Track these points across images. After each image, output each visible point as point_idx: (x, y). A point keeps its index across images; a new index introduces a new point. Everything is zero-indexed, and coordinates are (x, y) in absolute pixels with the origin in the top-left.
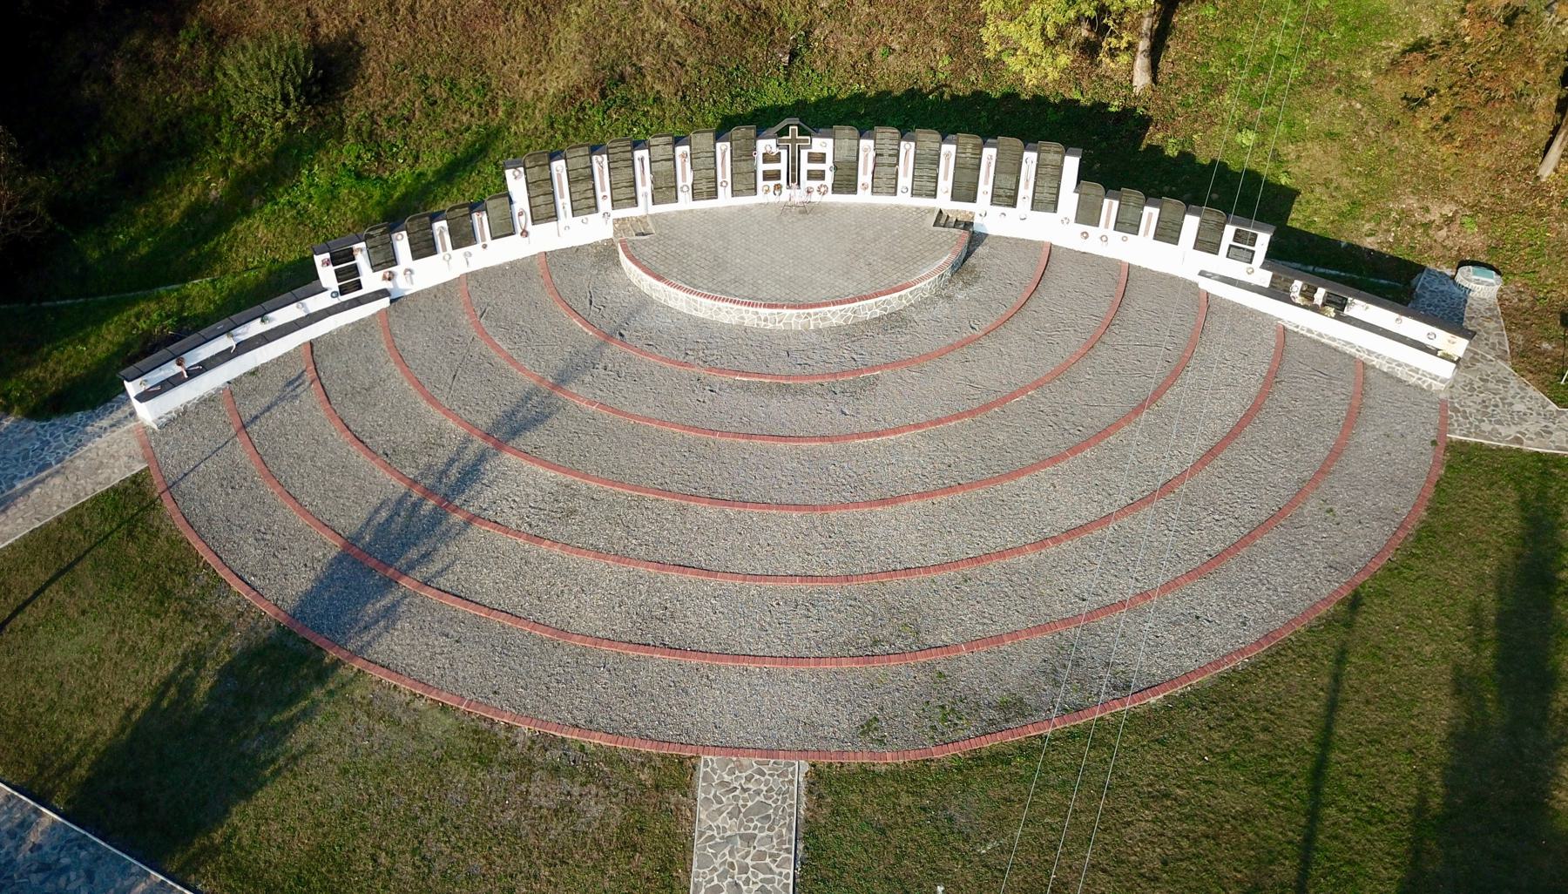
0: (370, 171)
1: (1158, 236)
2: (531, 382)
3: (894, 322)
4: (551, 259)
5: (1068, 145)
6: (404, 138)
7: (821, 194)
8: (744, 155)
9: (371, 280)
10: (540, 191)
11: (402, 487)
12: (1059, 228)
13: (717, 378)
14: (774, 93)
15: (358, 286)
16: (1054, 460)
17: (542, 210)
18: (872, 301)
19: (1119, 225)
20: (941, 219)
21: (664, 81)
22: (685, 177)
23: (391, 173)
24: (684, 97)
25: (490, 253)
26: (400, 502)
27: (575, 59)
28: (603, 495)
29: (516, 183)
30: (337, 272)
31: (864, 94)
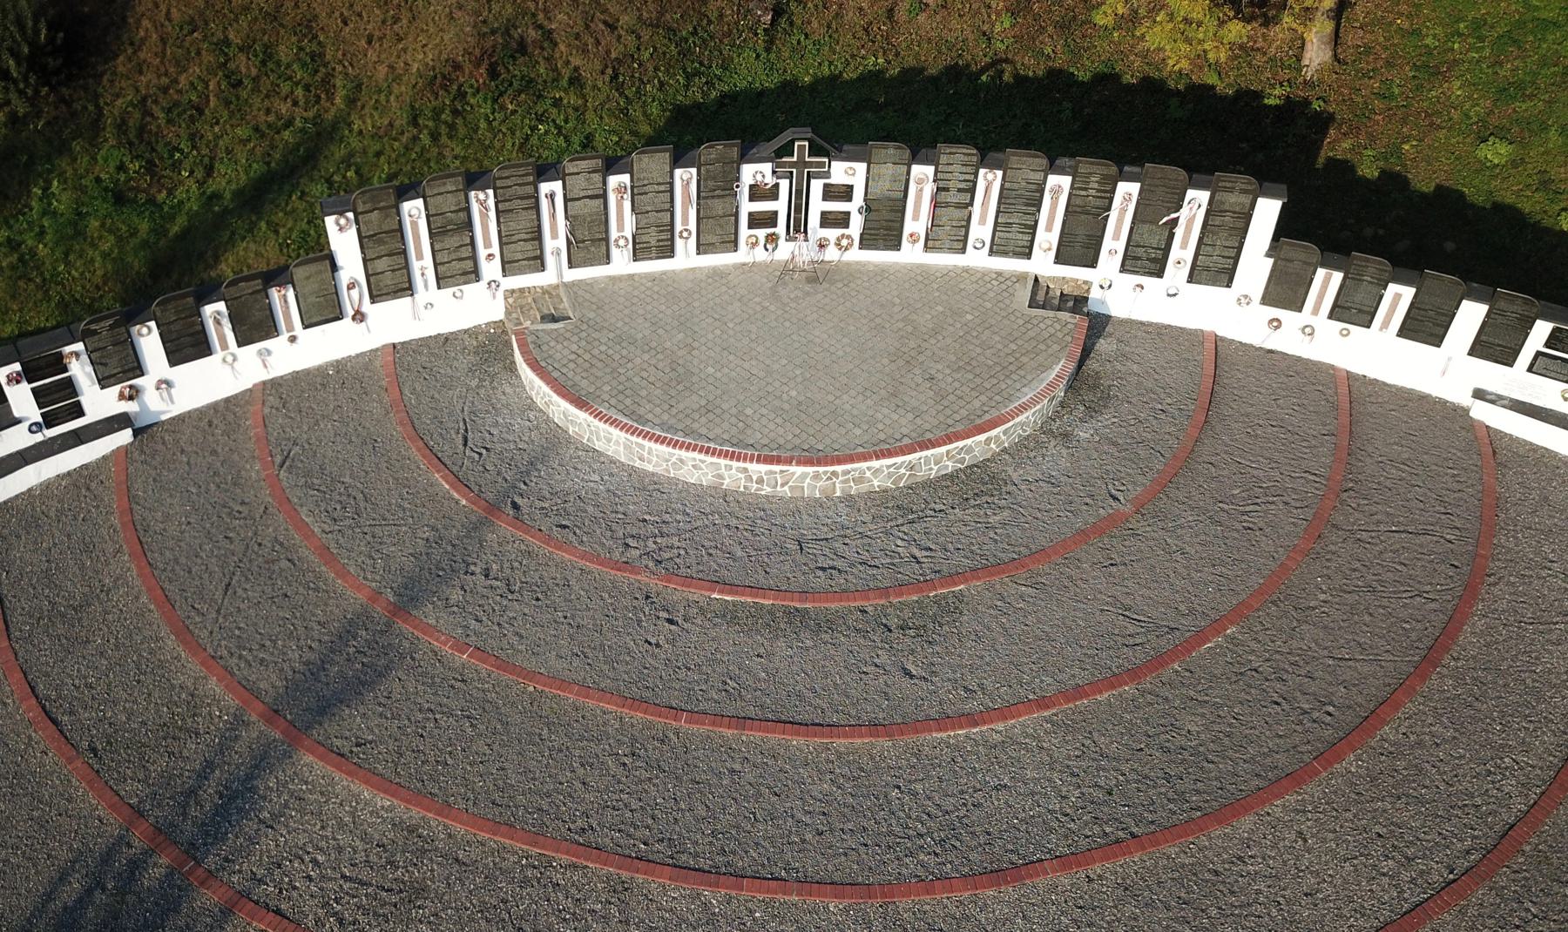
0: (137, 190)
1: (1406, 331)
2: (356, 598)
3: (976, 483)
5: (1266, 179)
6: (192, 137)
7: (847, 251)
8: (718, 189)
9: (99, 402)
10: (383, 249)
11: (114, 824)
12: (1236, 313)
13: (678, 594)
14: (750, 71)
15: (78, 411)
16: (1294, 779)
17: (388, 279)
18: (943, 449)
19: (1339, 311)
20: (1041, 296)
21: (585, 51)
22: (623, 222)
23: (170, 192)
24: (615, 77)
25: (301, 349)
26: (107, 858)
27: (451, 17)
28: (475, 853)
29: (343, 240)
30: (33, 390)
31: (881, 72)
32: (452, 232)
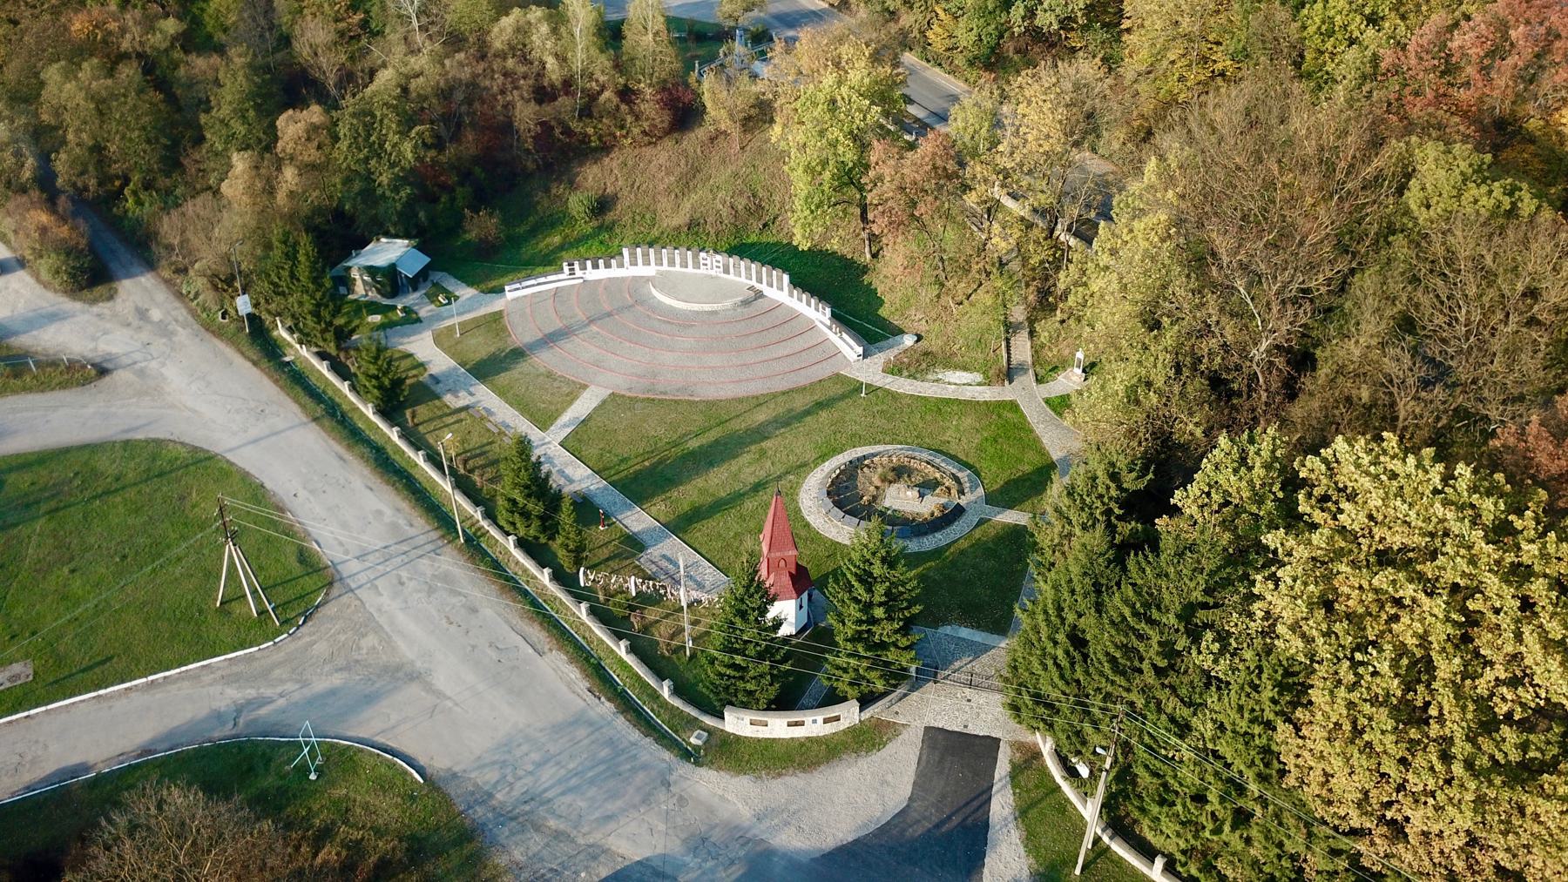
3: (714, 313)
4: (635, 278)
9: (578, 273)
29: (625, 252)
32: (646, 255)
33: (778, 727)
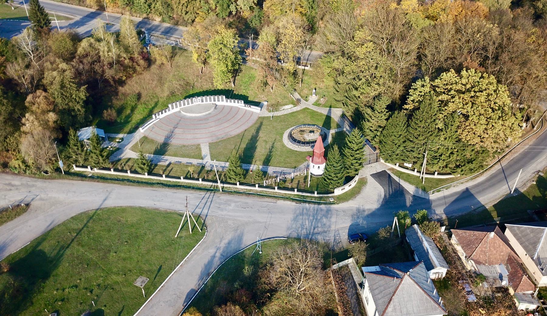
3: (210, 114)
8: (192, 100)
9: (158, 117)
25: (168, 113)
29: (170, 106)
33: (347, 188)
